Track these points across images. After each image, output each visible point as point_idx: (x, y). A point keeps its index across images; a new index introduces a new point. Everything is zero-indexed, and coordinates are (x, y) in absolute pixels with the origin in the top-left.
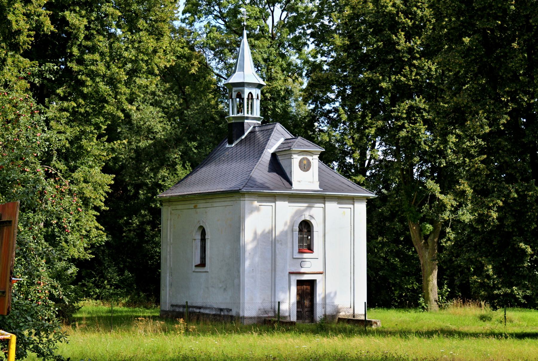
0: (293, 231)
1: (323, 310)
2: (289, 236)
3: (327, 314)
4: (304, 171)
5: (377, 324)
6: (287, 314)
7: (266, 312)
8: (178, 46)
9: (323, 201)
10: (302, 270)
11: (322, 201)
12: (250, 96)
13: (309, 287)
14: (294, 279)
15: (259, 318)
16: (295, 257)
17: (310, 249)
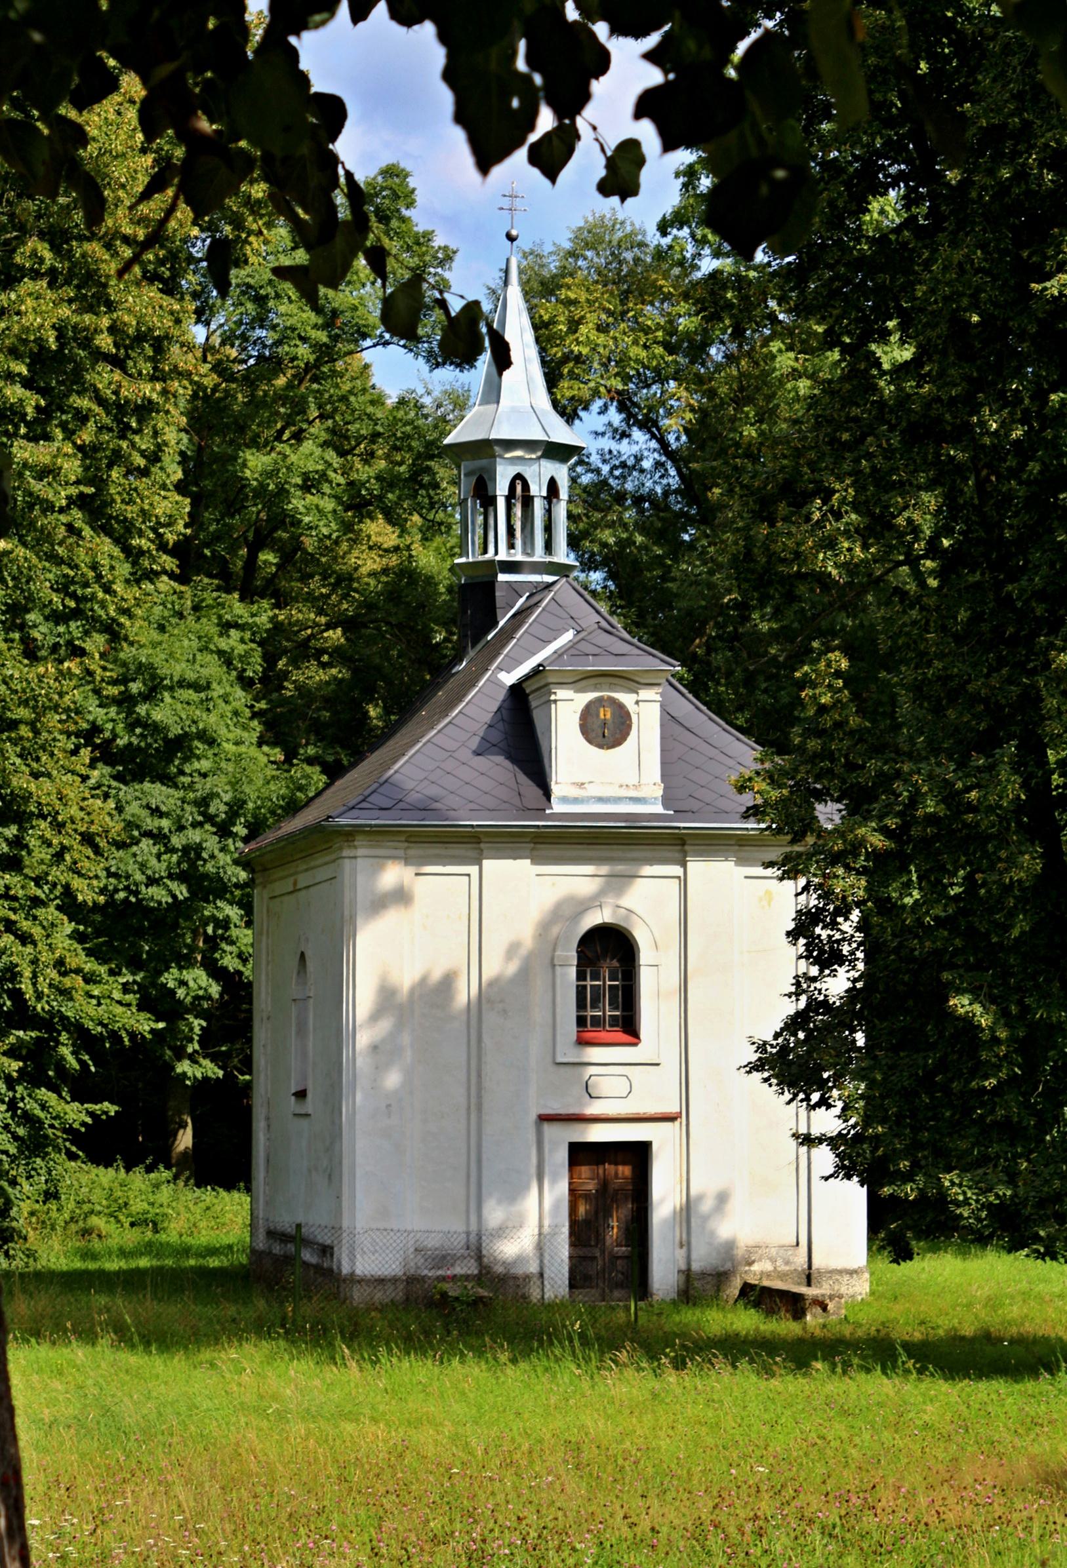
0: (553, 966)
1: (681, 1254)
2: (540, 983)
3: (696, 1266)
4: (601, 746)
5: (824, 1308)
6: (533, 1268)
7: (442, 1259)
8: (635, 342)
9: (677, 855)
10: (594, 1109)
11: (674, 853)
12: (519, 488)
13: (625, 1171)
14: (560, 1138)
15: (412, 1280)
16: (560, 1059)
17: (629, 1027)
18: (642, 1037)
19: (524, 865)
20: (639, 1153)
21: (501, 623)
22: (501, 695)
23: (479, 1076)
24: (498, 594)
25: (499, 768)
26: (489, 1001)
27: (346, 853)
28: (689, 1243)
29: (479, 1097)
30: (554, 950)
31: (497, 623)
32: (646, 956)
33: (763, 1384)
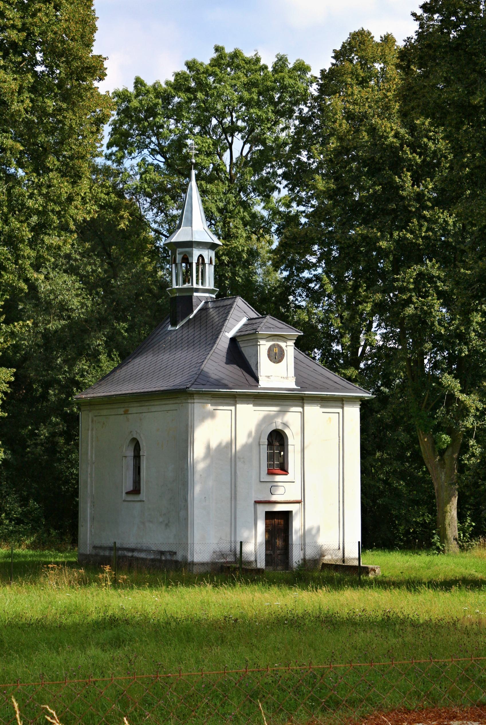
0: (260, 445)
1: (302, 553)
2: (255, 451)
3: (307, 557)
4: (274, 362)
9: (301, 404)
10: (274, 498)
14: (262, 510)
16: (262, 480)
17: (283, 469)
18: (289, 472)
19: (250, 406)
20: (287, 516)
21: (195, 312)
22: (228, 341)
23: (235, 486)
24: (193, 300)
25: (234, 370)
26: (239, 458)
27: (189, 401)
28: (305, 549)
29: (235, 494)
30: (260, 439)
31: (192, 312)
32: (291, 441)
33: (415, 598)
